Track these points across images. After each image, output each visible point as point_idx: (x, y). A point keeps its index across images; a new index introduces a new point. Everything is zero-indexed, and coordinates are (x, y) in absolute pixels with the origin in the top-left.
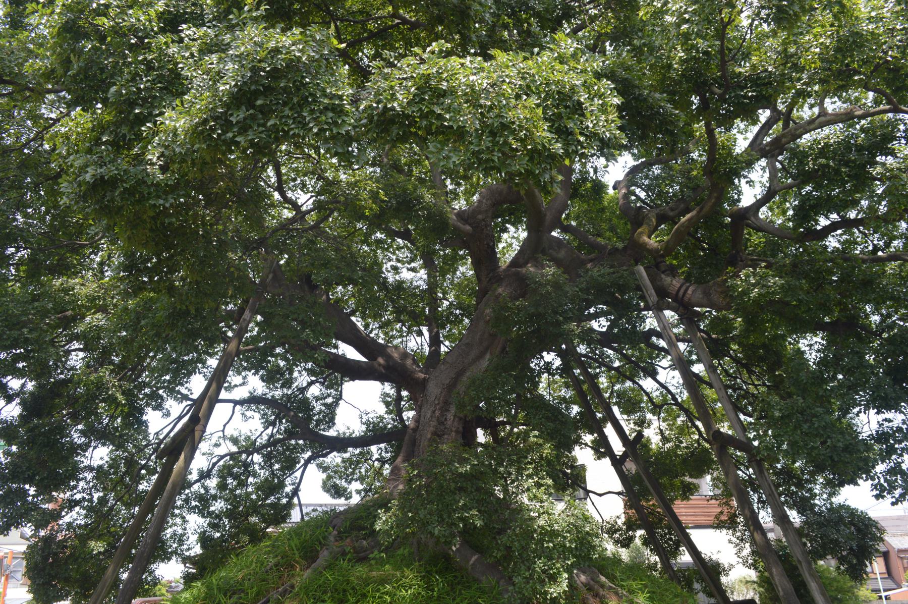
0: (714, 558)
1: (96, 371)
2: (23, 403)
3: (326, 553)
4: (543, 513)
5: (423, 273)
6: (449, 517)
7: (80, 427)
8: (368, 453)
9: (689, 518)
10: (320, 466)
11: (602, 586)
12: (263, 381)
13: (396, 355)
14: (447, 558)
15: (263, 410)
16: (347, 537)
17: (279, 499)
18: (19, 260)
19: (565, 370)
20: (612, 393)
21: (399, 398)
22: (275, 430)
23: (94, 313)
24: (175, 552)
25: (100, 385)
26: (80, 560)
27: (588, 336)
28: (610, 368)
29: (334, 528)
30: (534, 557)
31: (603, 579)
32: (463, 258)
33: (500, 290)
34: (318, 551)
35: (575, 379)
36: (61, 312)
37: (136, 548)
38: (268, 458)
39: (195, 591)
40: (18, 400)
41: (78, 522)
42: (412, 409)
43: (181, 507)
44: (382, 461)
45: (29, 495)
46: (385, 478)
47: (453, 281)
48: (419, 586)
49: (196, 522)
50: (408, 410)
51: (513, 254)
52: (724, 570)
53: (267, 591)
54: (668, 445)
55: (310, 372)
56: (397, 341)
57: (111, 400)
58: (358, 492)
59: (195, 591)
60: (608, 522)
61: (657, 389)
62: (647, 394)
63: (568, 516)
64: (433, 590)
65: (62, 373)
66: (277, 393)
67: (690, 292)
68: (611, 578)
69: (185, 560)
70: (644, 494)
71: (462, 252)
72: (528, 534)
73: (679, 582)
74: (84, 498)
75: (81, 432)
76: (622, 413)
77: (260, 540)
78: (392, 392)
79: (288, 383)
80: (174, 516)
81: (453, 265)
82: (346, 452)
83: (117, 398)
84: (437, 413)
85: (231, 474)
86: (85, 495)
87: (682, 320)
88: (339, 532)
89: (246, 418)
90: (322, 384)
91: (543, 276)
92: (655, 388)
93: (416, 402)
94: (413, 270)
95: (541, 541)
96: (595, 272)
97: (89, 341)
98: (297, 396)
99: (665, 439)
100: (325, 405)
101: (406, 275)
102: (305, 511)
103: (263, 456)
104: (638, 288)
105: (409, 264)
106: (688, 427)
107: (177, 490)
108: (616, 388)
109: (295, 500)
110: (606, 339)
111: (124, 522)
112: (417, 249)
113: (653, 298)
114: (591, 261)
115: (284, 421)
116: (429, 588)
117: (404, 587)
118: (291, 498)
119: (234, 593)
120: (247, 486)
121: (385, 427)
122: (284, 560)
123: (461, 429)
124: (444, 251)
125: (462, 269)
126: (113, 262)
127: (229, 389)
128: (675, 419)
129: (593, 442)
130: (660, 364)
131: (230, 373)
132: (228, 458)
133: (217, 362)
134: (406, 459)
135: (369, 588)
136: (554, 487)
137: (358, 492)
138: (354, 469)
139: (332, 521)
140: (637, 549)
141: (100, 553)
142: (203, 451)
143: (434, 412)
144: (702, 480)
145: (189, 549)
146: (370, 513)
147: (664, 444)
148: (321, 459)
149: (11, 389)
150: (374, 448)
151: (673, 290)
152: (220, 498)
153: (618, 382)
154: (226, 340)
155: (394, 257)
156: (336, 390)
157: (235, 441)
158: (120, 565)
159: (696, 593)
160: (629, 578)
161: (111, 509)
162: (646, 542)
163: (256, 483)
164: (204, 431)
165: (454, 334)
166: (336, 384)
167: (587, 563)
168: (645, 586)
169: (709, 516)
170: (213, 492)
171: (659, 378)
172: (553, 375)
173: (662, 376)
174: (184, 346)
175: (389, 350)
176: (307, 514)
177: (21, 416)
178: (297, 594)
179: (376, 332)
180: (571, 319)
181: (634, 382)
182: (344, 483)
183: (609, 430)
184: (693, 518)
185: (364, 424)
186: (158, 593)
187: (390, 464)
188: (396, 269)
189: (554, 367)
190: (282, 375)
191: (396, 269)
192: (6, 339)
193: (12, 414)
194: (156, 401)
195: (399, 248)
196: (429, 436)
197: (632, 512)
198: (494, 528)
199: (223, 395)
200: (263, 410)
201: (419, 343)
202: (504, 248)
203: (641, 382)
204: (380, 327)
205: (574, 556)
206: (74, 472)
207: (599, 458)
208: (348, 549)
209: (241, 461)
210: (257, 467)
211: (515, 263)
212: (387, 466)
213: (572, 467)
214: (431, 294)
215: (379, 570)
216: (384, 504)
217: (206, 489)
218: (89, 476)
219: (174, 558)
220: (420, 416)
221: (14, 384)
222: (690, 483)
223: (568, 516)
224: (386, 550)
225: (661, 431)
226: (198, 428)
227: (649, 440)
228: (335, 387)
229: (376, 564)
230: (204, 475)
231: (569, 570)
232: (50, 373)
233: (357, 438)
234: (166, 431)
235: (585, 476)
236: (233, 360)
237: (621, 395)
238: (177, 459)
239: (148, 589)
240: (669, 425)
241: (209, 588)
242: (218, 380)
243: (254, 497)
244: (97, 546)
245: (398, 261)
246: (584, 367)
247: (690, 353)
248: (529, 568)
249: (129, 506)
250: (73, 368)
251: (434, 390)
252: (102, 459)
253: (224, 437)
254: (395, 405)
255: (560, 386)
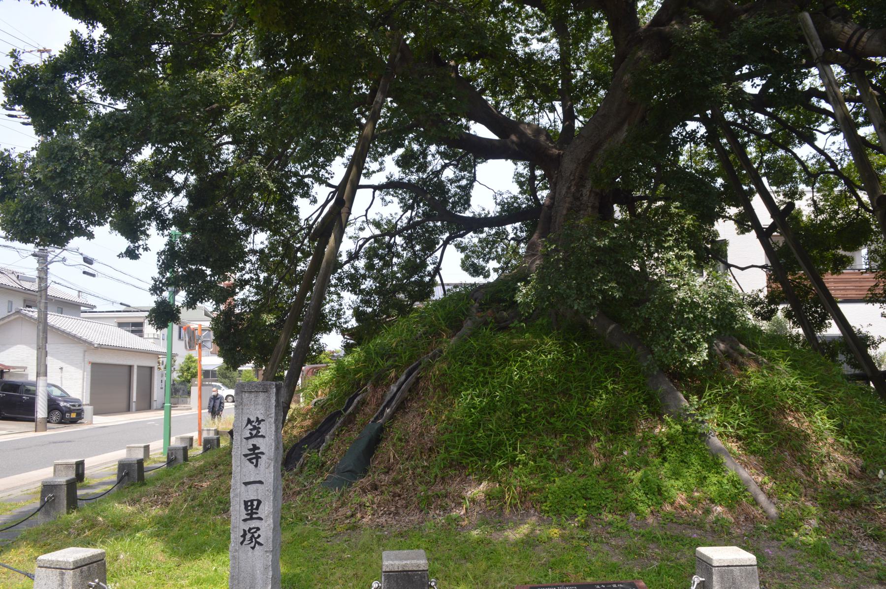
0: (864, 331)
1: (247, 161)
2: (188, 196)
3: (469, 322)
4: (684, 285)
5: (554, 43)
6: (588, 289)
7: (240, 215)
8: (504, 233)
9: (838, 292)
10: (458, 246)
11: (742, 354)
12: (399, 166)
13: (529, 132)
14: (585, 327)
15: (401, 194)
16: (488, 309)
17: (422, 277)
18: (164, 57)
19: (711, 139)
20: (761, 163)
21: (533, 177)
22: (414, 213)
23: (237, 104)
24: (334, 325)
25: (252, 175)
26: (256, 331)
27: (741, 101)
28: (760, 136)
29: (475, 301)
30: (673, 327)
31: (743, 347)
32: (598, 21)
33: (640, 54)
34: (461, 321)
35: (720, 148)
36: (209, 106)
37: (301, 321)
38: (409, 240)
39: (356, 355)
40: (184, 192)
41: (251, 298)
42: (546, 188)
43: (336, 286)
44: (518, 240)
45: (207, 276)
46: (521, 256)
47: (587, 49)
48: (558, 352)
49: (349, 298)
50: (542, 190)
51: (653, 13)
52: (874, 343)
53: (419, 356)
54: (821, 217)
55: (443, 155)
56: (529, 119)
57: (263, 189)
58: (496, 270)
59: (356, 355)
60: (749, 296)
61: (814, 157)
62: (802, 163)
63: (710, 287)
64: (572, 356)
65: (217, 167)
66: (413, 177)
67: (864, 39)
68: (752, 346)
69: (344, 332)
70: (792, 267)
71: (596, 16)
72: (667, 306)
73: (823, 354)
74: (252, 278)
75: (241, 219)
76: (770, 185)
77: (409, 313)
78: (526, 172)
79: (423, 167)
80: (330, 293)
81: (586, 31)
82: (482, 232)
83: (268, 186)
84: (573, 189)
85: (377, 255)
86: (252, 275)
87: (849, 78)
88: (481, 304)
89: (385, 203)
90: (456, 166)
91: (689, 32)
92: (811, 156)
93: (551, 179)
94: (544, 40)
95: (680, 313)
96: (751, 24)
97: (237, 132)
98: (432, 179)
99: (818, 211)
100: (459, 187)
101: (536, 46)
102: (446, 288)
103: (405, 238)
104: (802, 39)
105: (539, 33)
106: (846, 197)
107: (331, 268)
108: (765, 158)
109: (437, 278)
110: (759, 102)
111: (288, 299)
112: (547, 15)
113: (817, 48)
114: (746, 11)
115: (421, 204)
116: (568, 353)
117: (544, 353)
118: (433, 277)
119: (390, 357)
120: (392, 266)
121: (520, 207)
122: (432, 329)
123: (597, 204)
124: (577, 15)
125: (596, 35)
126: (247, 54)
127: (368, 175)
128: (832, 189)
129: (737, 215)
130: (819, 128)
131: (368, 159)
132: (372, 240)
133: (354, 149)
134: (543, 235)
135: (511, 353)
136: (696, 258)
137: (496, 270)
138: (491, 249)
139: (473, 295)
140: (779, 323)
141: (271, 324)
142: (350, 234)
143: (569, 188)
144: (856, 253)
145: (346, 322)
146: (509, 287)
147: (816, 217)
148: (459, 239)
149: (177, 182)
150: (509, 228)
151: (843, 39)
152: (369, 277)
153: (768, 151)
154: (362, 127)
155: (523, 28)
156: (470, 172)
157: (377, 224)
158: (291, 335)
159: (840, 365)
160: (770, 347)
161: (276, 287)
162: (788, 315)
163: (399, 264)
164: (349, 213)
165: (588, 108)
166: (470, 166)
167: (728, 333)
168: (787, 355)
169: (861, 290)
170: (362, 272)
171: (816, 143)
172: (697, 144)
173: (821, 141)
174: (321, 128)
175: (522, 127)
176: (449, 290)
177: (188, 207)
178: (446, 358)
179: (507, 110)
180: (720, 80)
181: (788, 150)
182: (481, 262)
183: (757, 202)
184: (843, 292)
185: (499, 204)
186: (323, 361)
187: (525, 243)
188: (525, 41)
189: (699, 135)
190: (417, 159)
191: (525, 41)
192: (165, 133)
193: (181, 204)
194: (303, 189)
195: (528, 17)
196: (565, 212)
197: (777, 286)
198: (632, 299)
199: (363, 181)
200: (401, 194)
201: (552, 120)
202: (643, 7)
203: (795, 150)
204: (511, 105)
205: (715, 327)
206: (241, 255)
207: (742, 232)
208: (489, 320)
209: (384, 243)
210: (400, 249)
211: (656, 21)
212: (522, 245)
213: (713, 242)
214: (564, 64)
215: (520, 338)
216: (523, 277)
217: (356, 269)
218: (254, 258)
219: (334, 330)
220: (555, 193)
221: (179, 178)
222: (843, 257)
223: (710, 287)
224: (526, 320)
225: (814, 202)
226: (344, 210)
227: (799, 212)
228: (469, 169)
229: (517, 332)
230: (353, 256)
231: (708, 340)
232: (207, 167)
233: (495, 218)
234: (314, 217)
235: (726, 251)
236: (369, 147)
237: (770, 165)
238: (327, 243)
239: (315, 356)
240: (823, 196)
241: (368, 352)
242: (356, 166)
243: (399, 275)
244: (269, 319)
245: (527, 31)
246: (733, 137)
247: (856, 115)
248: (668, 338)
249: (291, 285)
250: (226, 162)
251: (569, 166)
252: (262, 243)
253: (367, 222)
254: (529, 184)
255: (703, 158)
